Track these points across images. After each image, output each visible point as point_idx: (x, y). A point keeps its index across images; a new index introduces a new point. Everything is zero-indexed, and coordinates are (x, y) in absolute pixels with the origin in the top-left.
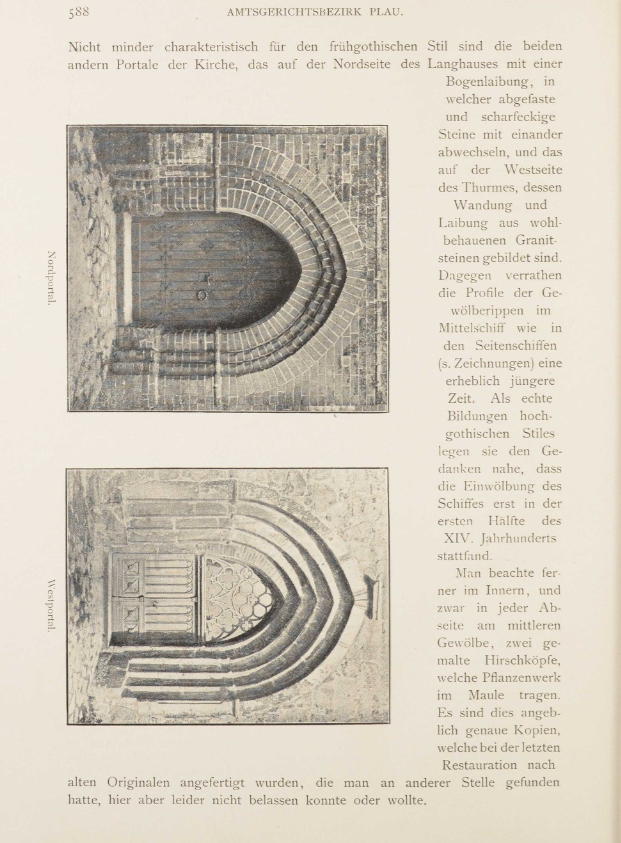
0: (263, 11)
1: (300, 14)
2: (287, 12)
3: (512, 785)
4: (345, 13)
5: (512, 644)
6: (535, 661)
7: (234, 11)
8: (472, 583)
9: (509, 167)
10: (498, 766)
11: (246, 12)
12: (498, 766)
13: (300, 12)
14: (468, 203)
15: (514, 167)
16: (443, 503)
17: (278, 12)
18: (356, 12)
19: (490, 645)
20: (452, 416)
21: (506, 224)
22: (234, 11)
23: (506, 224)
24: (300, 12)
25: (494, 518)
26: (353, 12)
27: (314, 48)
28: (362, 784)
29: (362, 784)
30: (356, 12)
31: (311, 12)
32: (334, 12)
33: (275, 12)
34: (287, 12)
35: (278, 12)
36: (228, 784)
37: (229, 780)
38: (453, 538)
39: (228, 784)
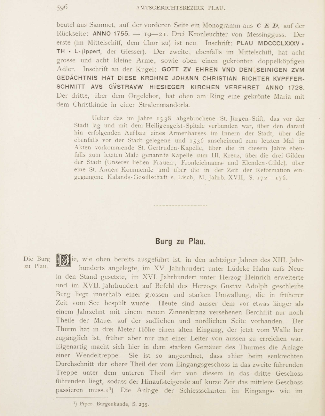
0: (154, 7)
1: (173, 8)
2: (166, 7)
3: (275, 288)
4: (196, 8)
5: (255, 365)
6: (284, 62)
7: (140, 7)
8: (178, 39)
9: (275, 328)
10: (282, 171)
11: (146, 7)
12: (282, 171)
13: (173, 7)
14: (280, 328)
15: (277, 328)
16: (58, 294)
17: (162, 7)
18: (202, 8)
19: (188, 53)
20: (58, 294)
21: (276, 269)
22: (140, 7)
23: (276, 269)
24: (173, 7)
25: (161, 302)
26: (200, 8)
27: (195, 61)
28: (171, 357)
29: (171, 357)
30: (202, 8)
31: (179, 8)
32: (190, 8)
33: (160, 7)
34: (166, 7)
35: (162, 7)
36: (81, 347)
37: (82, 345)
38: (277, 260)
39: (81, 347)
